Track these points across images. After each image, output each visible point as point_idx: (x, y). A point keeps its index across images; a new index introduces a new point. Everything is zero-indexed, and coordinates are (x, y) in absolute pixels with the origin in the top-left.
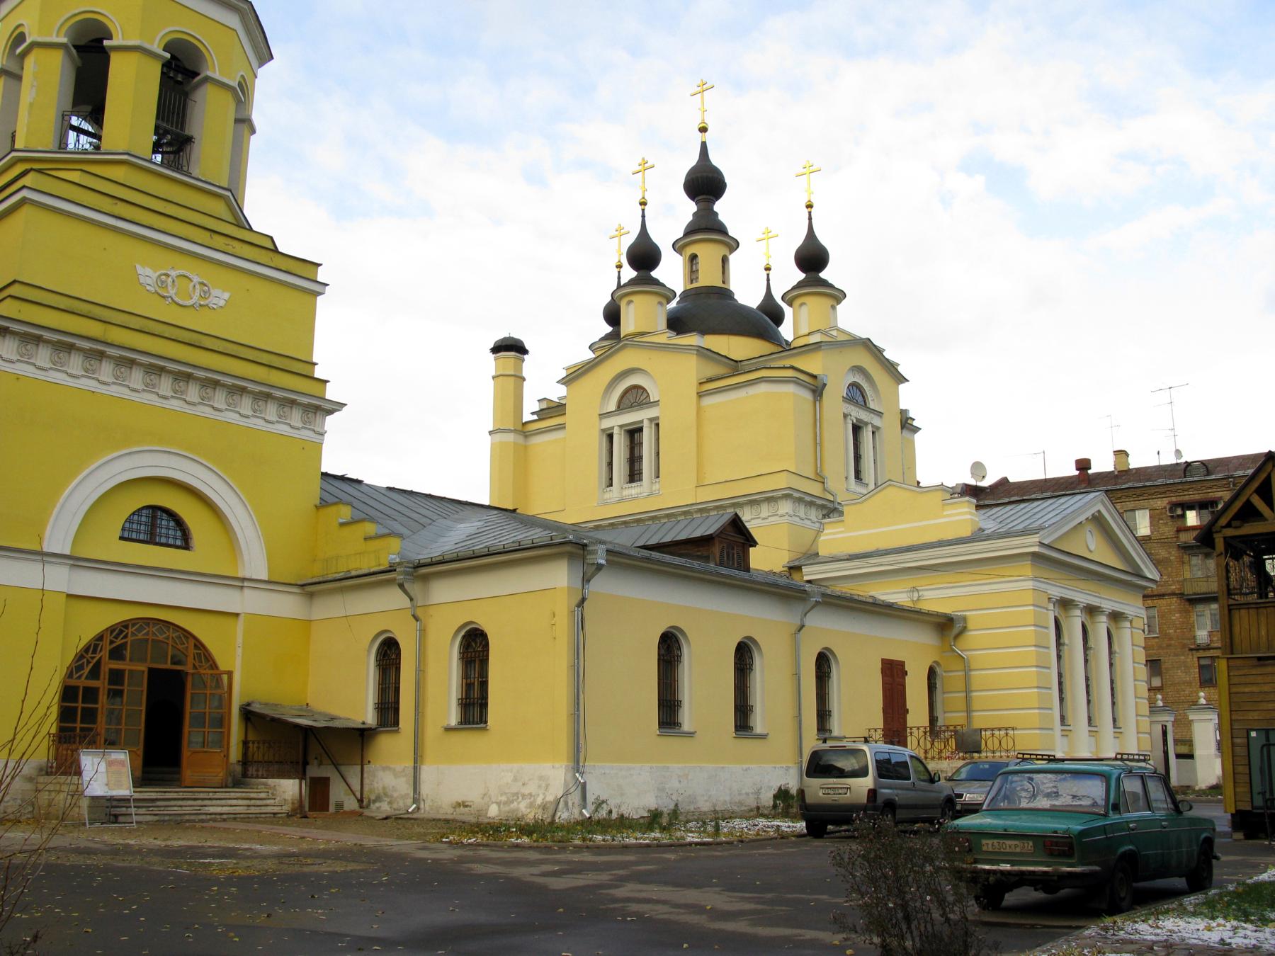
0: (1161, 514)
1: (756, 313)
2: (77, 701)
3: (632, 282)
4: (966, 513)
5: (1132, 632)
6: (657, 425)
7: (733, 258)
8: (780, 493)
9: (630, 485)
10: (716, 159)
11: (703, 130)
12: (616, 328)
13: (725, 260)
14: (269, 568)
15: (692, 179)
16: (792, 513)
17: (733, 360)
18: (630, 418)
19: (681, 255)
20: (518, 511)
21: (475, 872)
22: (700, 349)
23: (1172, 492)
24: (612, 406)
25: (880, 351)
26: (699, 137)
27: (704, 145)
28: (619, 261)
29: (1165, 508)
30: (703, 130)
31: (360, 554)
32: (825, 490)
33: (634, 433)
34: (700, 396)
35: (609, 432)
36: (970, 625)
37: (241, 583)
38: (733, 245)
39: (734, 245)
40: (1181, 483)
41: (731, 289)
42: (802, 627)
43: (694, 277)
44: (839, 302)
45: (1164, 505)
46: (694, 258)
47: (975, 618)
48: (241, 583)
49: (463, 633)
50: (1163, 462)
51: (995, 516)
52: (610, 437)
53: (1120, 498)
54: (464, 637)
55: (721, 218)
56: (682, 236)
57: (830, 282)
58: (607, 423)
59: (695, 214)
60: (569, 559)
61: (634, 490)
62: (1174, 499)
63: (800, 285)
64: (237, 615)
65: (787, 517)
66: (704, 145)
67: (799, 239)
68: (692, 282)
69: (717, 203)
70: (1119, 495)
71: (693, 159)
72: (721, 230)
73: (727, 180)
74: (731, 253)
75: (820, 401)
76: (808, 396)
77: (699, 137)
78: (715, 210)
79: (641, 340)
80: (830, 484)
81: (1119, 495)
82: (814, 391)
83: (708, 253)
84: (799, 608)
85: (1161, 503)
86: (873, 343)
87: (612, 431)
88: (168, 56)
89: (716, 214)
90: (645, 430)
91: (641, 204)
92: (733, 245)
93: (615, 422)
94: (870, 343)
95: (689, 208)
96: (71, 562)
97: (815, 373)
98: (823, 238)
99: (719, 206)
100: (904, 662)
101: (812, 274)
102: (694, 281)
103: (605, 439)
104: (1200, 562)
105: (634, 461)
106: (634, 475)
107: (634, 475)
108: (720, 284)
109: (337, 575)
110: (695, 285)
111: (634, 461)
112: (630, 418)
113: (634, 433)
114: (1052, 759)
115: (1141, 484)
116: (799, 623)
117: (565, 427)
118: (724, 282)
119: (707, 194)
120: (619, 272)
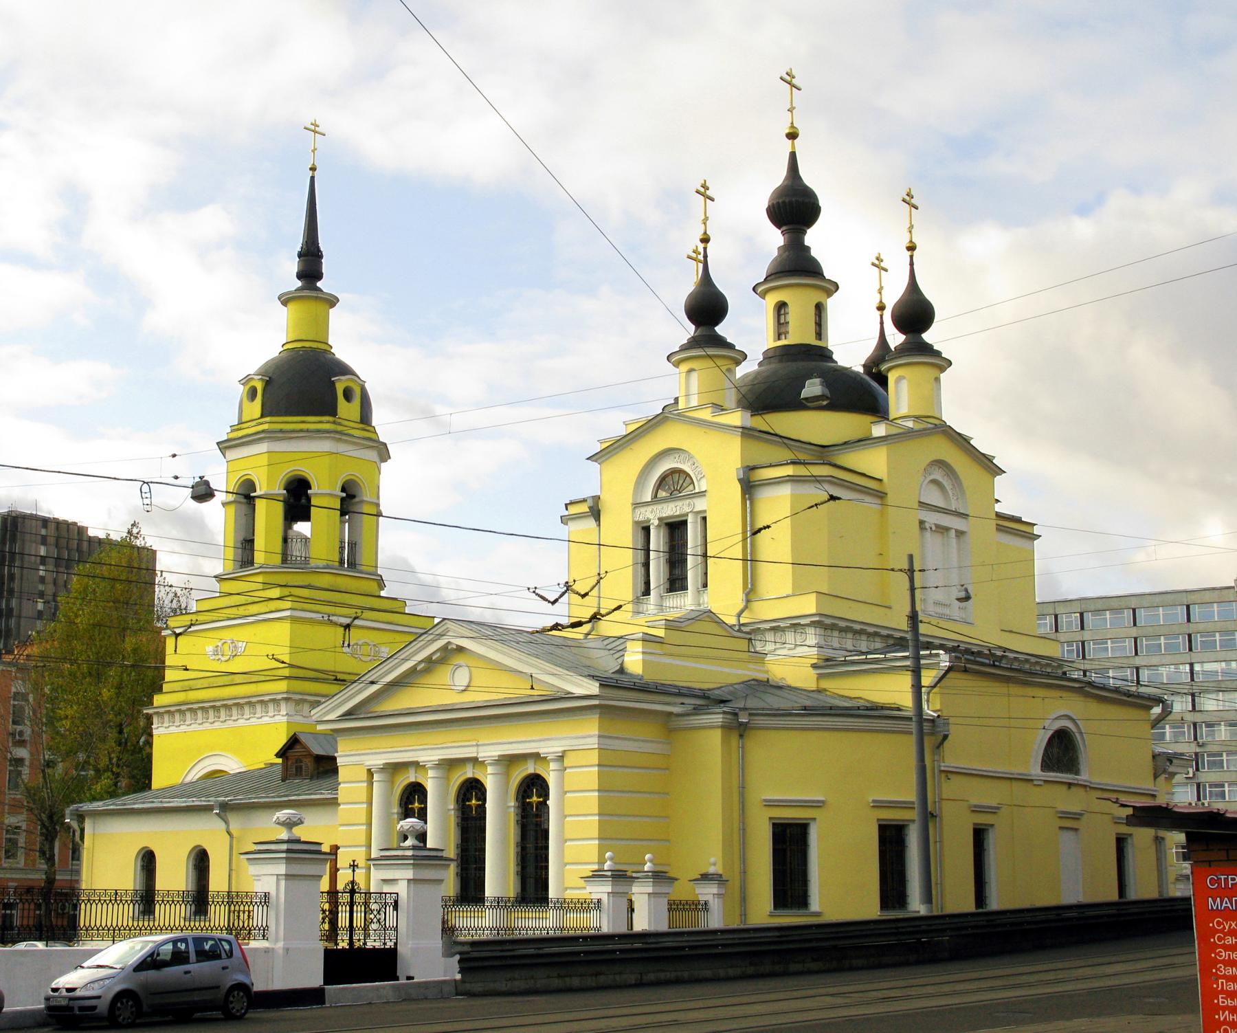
1: (862, 378)
6: (705, 519)
7: (832, 304)
8: (767, 626)
11: (792, 136)
13: (820, 309)
14: (470, 650)
15: (773, 205)
18: (671, 510)
24: (648, 497)
25: (965, 440)
28: (911, 242)
30: (792, 136)
33: (676, 528)
34: (353, 565)
35: (645, 525)
39: (833, 288)
43: (782, 330)
44: (943, 369)
46: (781, 307)
52: (646, 530)
55: (814, 253)
56: (763, 280)
66: (793, 157)
69: (809, 231)
70: (1027, 666)
71: (778, 177)
73: (822, 203)
78: (806, 244)
83: (799, 300)
86: (955, 431)
87: (684, 518)
89: (808, 249)
90: (690, 526)
93: (653, 515)
94: (951, 432)
95: (774, 239)
98: (929, 291)
99: (814, 238)
100: (331, 846)
102: (783, 336)
103: (640, 535)
106: (676, 583)
107: (676, 583)
108: (811, 340)
114: (1042, 981)
117: (705, 495)
120: (911, 257)
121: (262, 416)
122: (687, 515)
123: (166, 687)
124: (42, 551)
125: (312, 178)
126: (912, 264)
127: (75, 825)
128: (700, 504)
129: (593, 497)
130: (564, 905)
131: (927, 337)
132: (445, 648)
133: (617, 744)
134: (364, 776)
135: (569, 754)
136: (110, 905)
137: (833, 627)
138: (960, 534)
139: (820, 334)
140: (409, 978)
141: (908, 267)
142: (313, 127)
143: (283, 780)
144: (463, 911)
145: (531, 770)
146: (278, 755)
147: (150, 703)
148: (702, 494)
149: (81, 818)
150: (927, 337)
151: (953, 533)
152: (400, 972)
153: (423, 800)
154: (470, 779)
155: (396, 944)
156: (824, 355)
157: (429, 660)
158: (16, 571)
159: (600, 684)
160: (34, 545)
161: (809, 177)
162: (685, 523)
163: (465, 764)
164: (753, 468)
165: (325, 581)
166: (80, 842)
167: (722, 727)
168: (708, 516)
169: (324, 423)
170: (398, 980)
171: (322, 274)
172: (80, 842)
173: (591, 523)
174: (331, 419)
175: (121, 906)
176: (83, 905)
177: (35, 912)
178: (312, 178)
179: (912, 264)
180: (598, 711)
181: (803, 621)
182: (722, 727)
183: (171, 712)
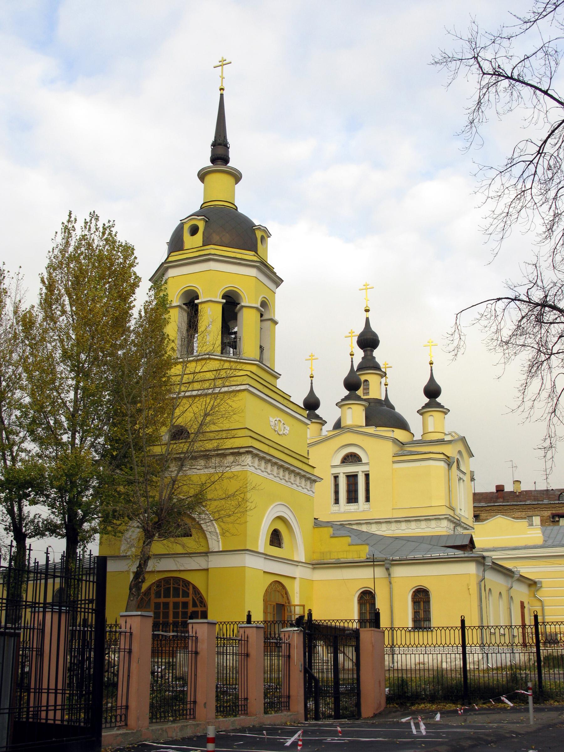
0: (547, 519)
2: (179, 618)
4: (539, 533)
9: (348, 504)
10: (374, 327)
17: (401, 442)
20: (319, 519)
22: (395, 440)
23: (553, 508)
26: (365, 315)
27: (367, 319)
29: (549, 516)
30: (367, 311)
31: (347, 551)
32: (454, 514)
36: (544, 585)
37: (296, 563)
40: (559, 503)
42: (511, 587)
45: (548, 514)
47: (545, 582)
48: (296, 563)
49: (414, 590)
50: (538, 488)
53: (525, 509)
54: (414, 592)
55: (377, 360)
58: (335, 471)
59: (363, 358)
60: (476, 563)
61: (352, 507)
62: (554, 512)
64: (295, 578)
65: (445, 529)
66: (367, 319)
67: (425, 381)
72: (377, 367)
76: (446, 466)
77: (365, 315)
79: (358, 430)
80: (458, 512)
81: (525, 508)
82: (449, 465)
84: (510, 581)
85: (547, 513)
88: (224, 301)
89: (374, 358)
96: (264, 556)
97: (449, 455)
109: (331, 560)
112: (351, 469)
115: (536, 503)
116: (510, 586)
119: (371, 347)
121: (204, 245)
125: (222, 95)
171: (229, 158)
178: (222, 95)
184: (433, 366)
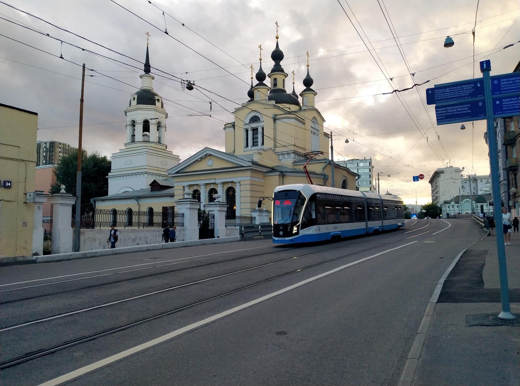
3: (257, 85)
5: (25, 191)
11: (277, 38)
12: (253, 98)
13: (284, 80)
16: (294, 157)
18: (254, 125)
19: (270, 78)
21: (17, 261)
30: (277, 38)
38: (286, 76)
41: (286, 90)
51: (248, 157)
52: (247, 131)
56: (270, 72)
57: (266, 84)
58: (247, 127)
59: (274, 66)
63: (305, 91)
68: (274, 87)
71: (274, 48)
72: (282, 71)
74: (286, 78)
75: (275, 123)
78: (280, 64)
91: (260, 60)
92: (286, 76)
93: (249, 127)
95: (272, 63)
98: (312, 76)
99: (282, 63)
101: (261, 82)
104: (89, 167)
105: (255, 139)
106: (255, 144)
110: (275, 88)
111: (255, 139)
112: (254, 125)
113: (255, 130)
118: (284, 87)
121: (137, 104)
122: (258, 127)
123: (111, 171)
124: (60, 150)
125: (148, 47)
126: (308, 70)
127: (93, 203)
128: (261, 124)
129: (233, 122)
130: (241, 217)
131: (311, 87)
132: (206, 155)
133: (254, 179)
134: (182, 188)
135: (241, 181)
136: (102, 221)
137: (297, 154)
138: (317, 135)
139: (284, 87)
140: (218, 237)
141: (307, 70)
142: (147, 34)
143: (151, 191)
144: (488, 213)
145: (230, 186)
146: (150, 185)
147: (108, 175)
148: (263, 121)
149: (95, 202)
150: (311, 87)
151: (316, 134)
152: (216, 235)
153: (199, 194)
154: (195, 190)
155: (214, 228)
156: (285, 91)
157: (201, 158)
158: (54, 154)
159: (252, 163)
160: (57, 148)
161: (281, 48)
162: (258, 129)
163: (194, 186)
164: (277, 115)
165: (153, 145)
166: (95, 208)
167: (279, 175)
168: (264, 127)
169: (153, 107)
170: (215, 238)
172: (95, 208)
173: (232, 129)
174: (155, 106)
175: (98, 221)
176: (111, 222)
177: (166, 221)
178: (148, 47)
179: (308, 70)
180: (250, 170)
181: (284, 153)
182: (279, 175)
183: (113, 177)
184: (309, 67)
